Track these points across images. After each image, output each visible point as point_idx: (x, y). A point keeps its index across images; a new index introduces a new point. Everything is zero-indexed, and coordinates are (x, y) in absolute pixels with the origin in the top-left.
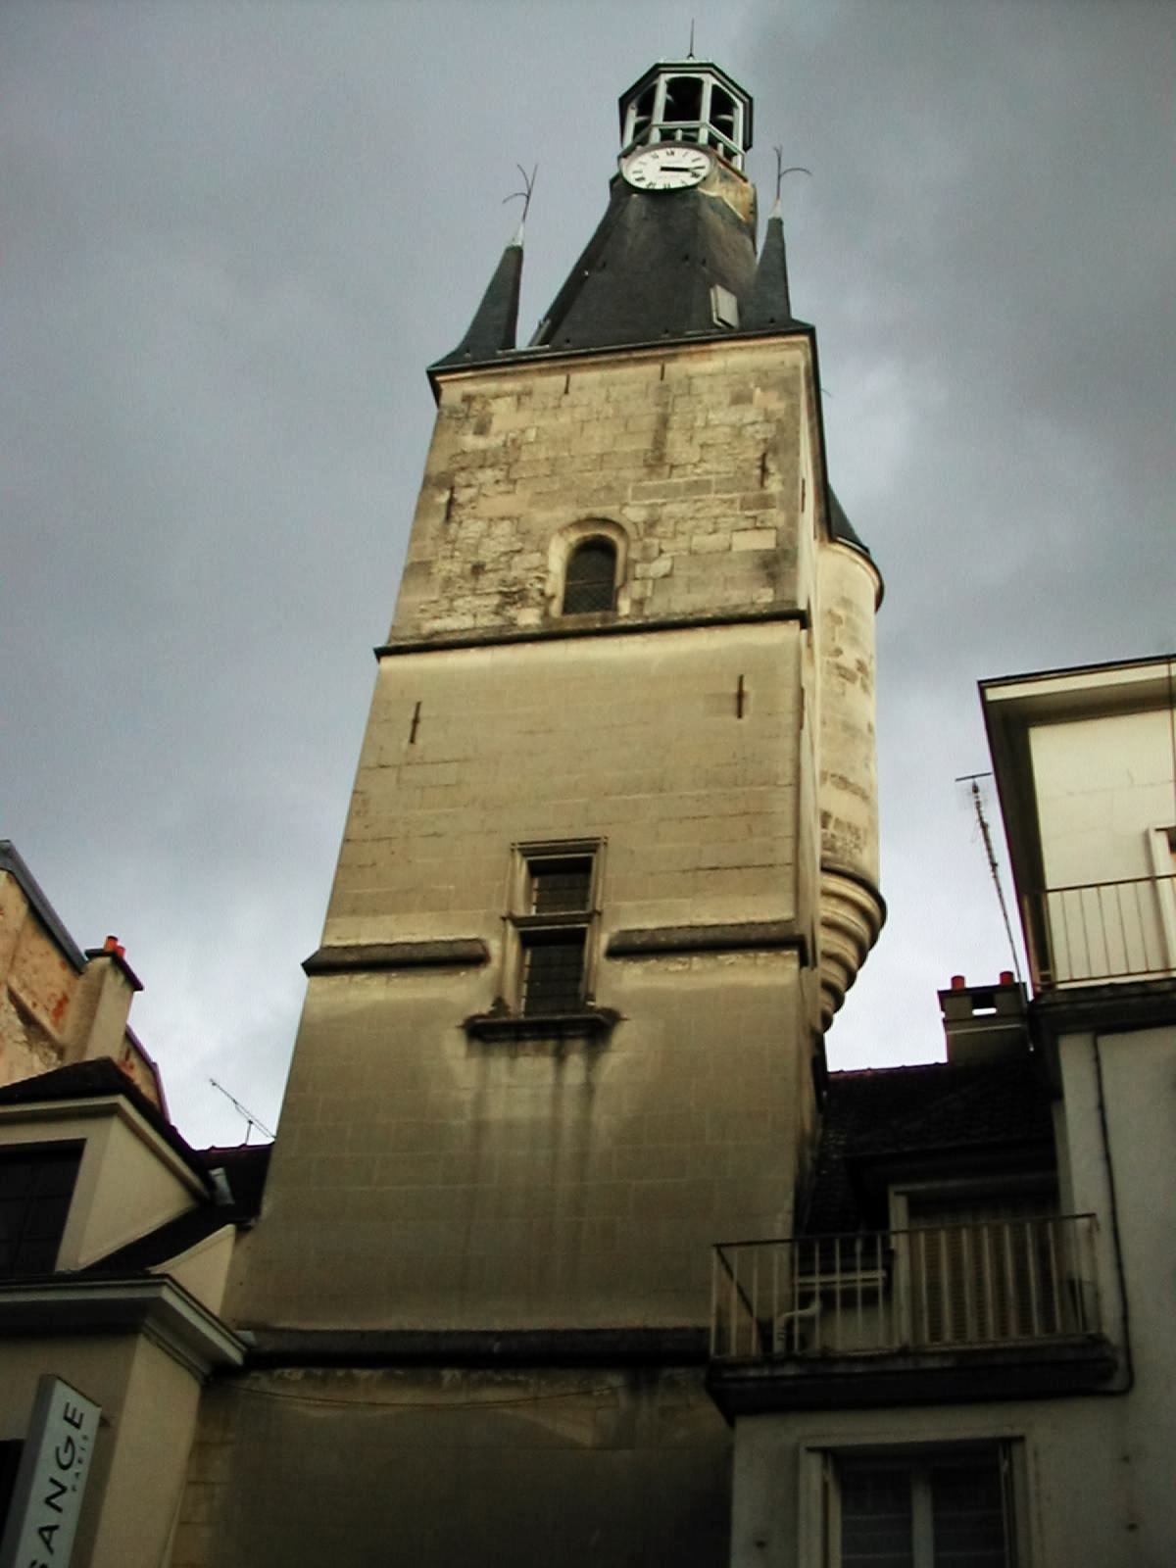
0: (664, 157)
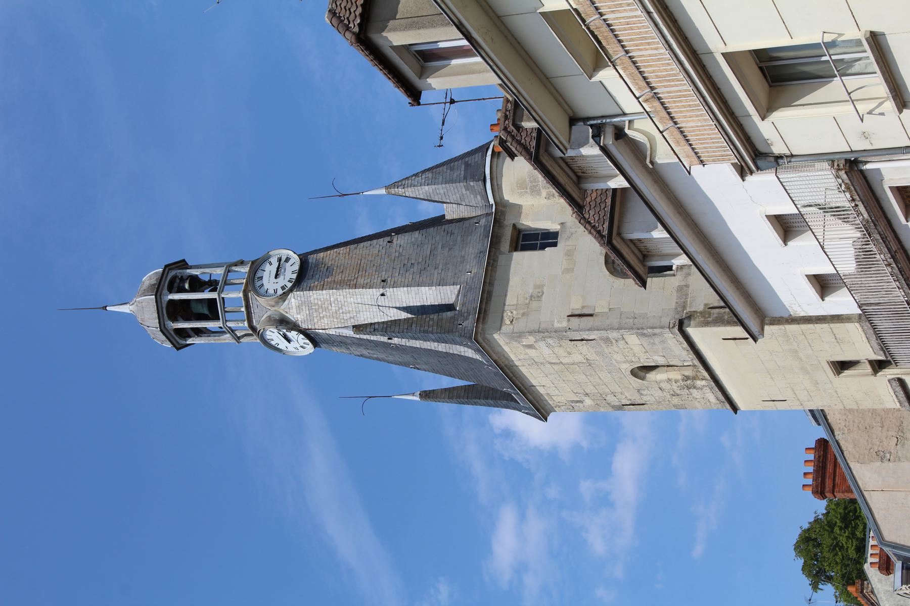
0: (291, 348)
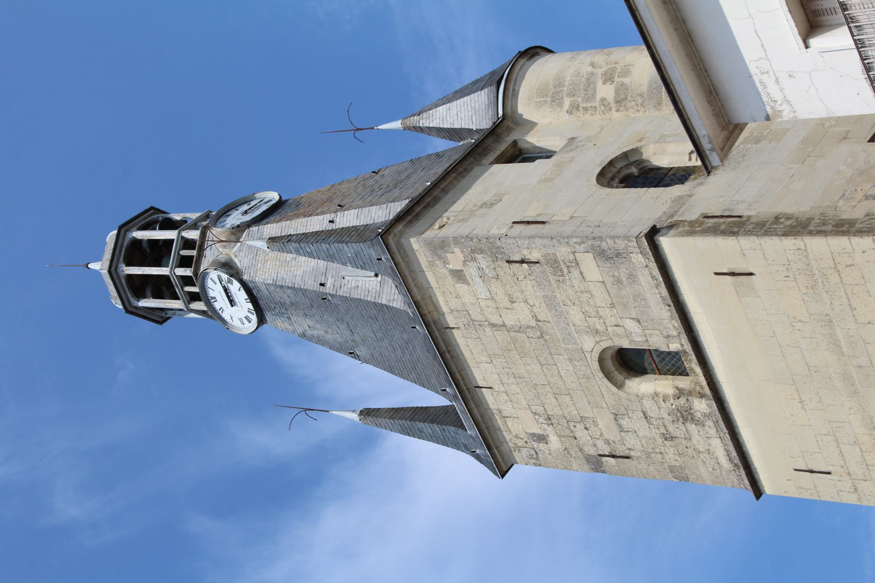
0: (227, 312)
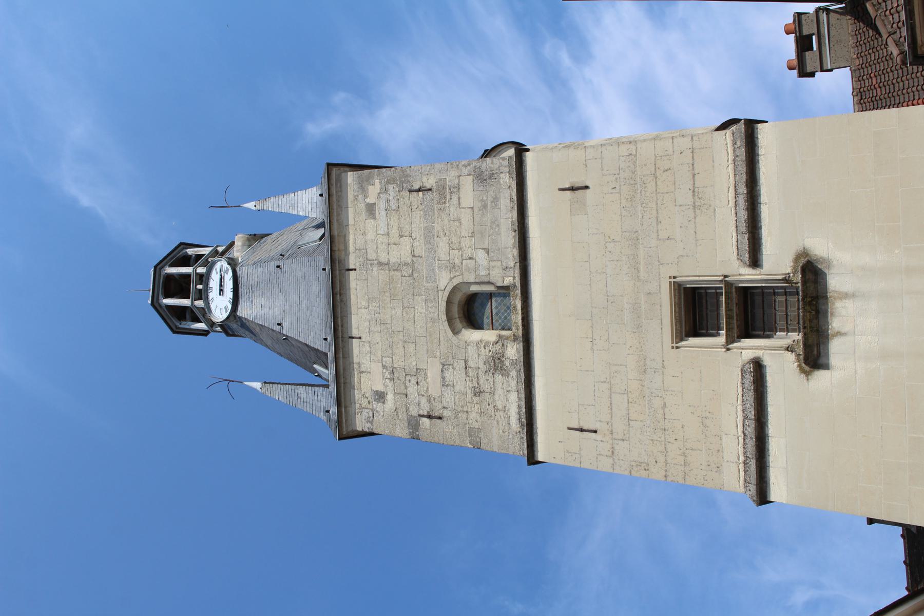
0: (213, 294)
